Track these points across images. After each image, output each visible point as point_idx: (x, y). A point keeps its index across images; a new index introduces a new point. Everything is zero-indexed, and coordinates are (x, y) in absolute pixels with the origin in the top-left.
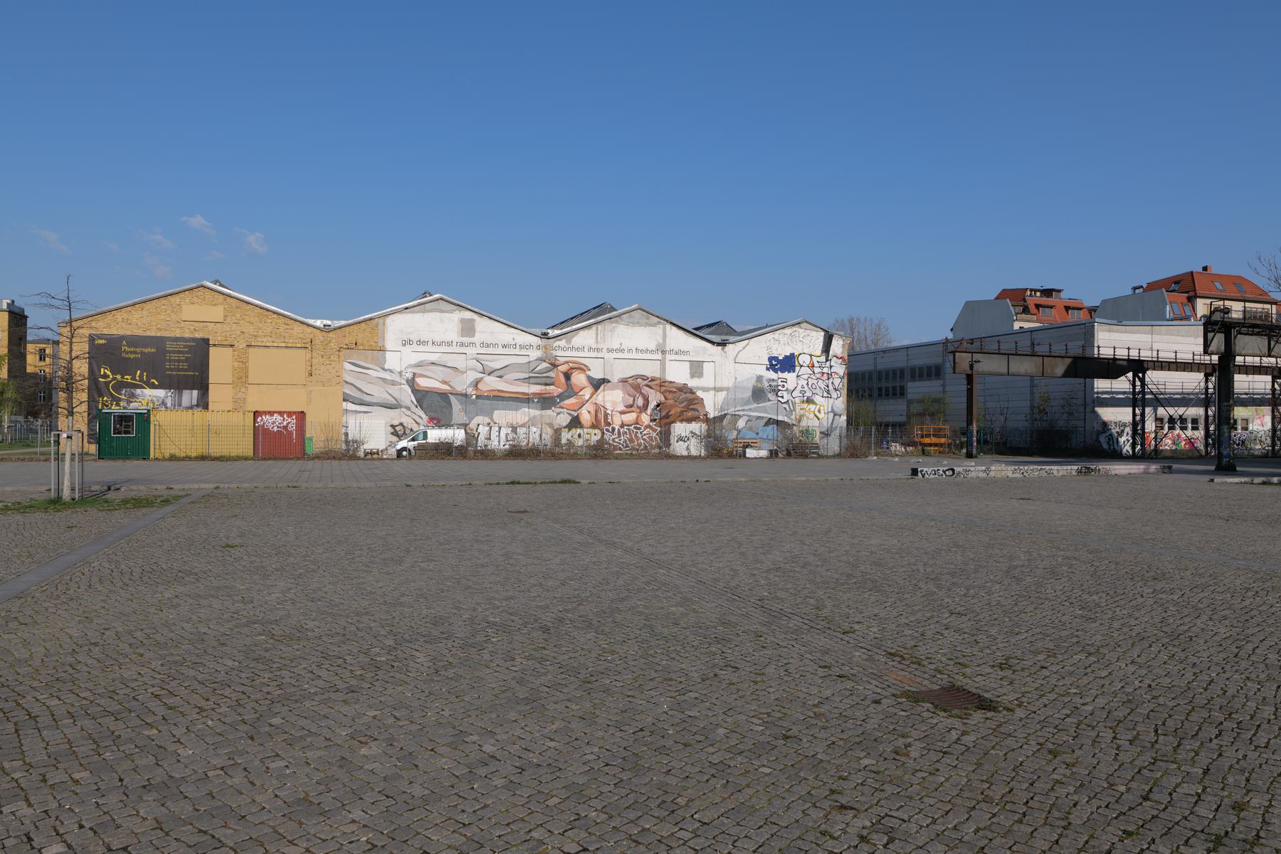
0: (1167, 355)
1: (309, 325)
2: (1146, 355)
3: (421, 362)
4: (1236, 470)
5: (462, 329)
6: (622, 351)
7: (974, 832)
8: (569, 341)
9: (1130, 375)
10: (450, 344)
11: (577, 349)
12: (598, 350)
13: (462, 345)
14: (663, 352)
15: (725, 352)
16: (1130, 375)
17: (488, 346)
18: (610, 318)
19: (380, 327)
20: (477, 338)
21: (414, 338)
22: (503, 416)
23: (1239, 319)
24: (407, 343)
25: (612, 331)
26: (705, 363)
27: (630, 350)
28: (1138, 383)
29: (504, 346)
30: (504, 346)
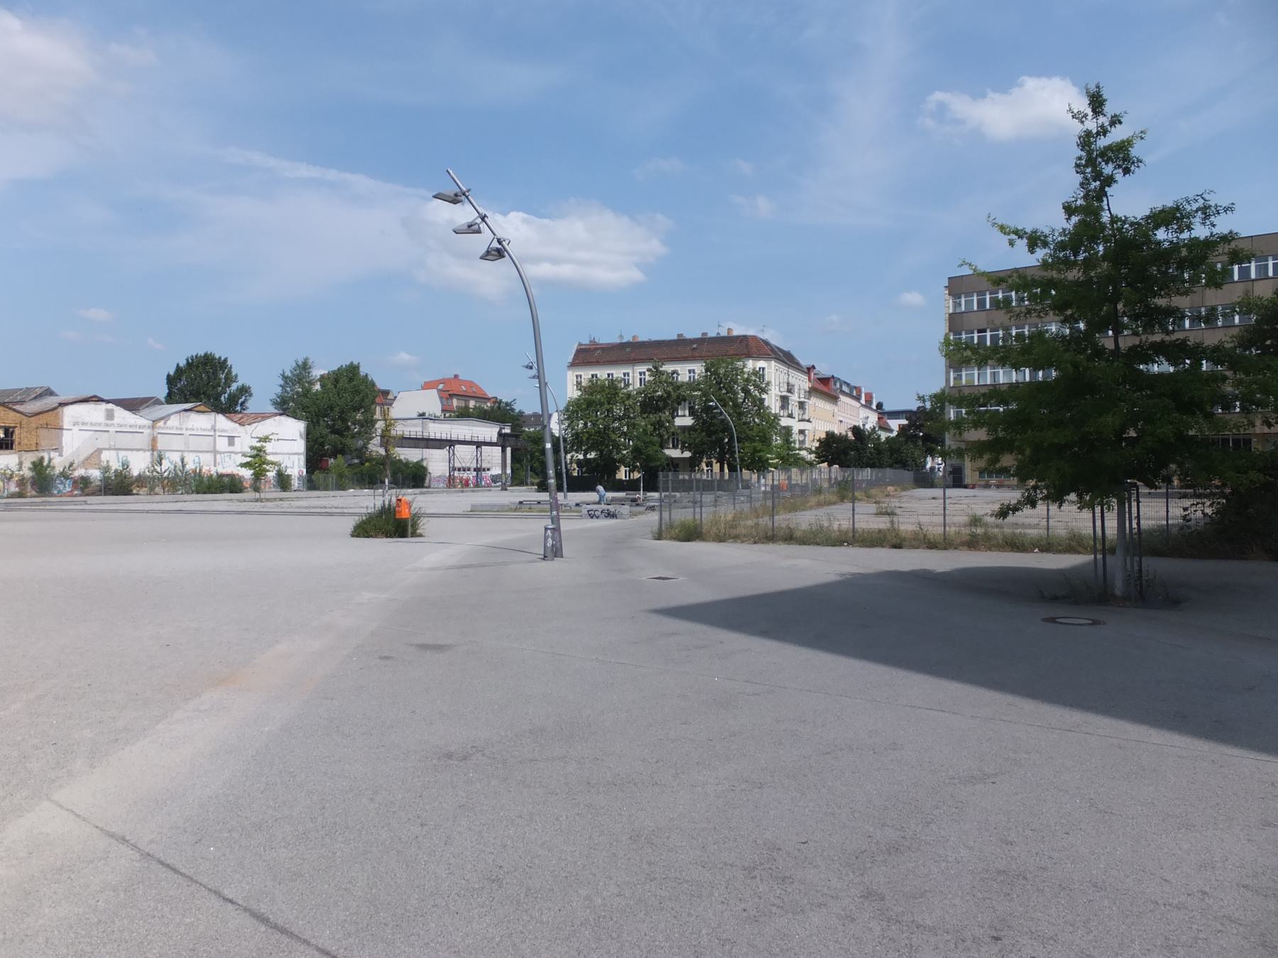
0: (461, 438)
1: (15, 410)
2: (454, 437)
3: (22, 404)
4: (537, 485)
5: (107, 415)
6: (193, 430)
7: (893, 939)
8: (165, 423)
9: (448, 448)
10: (100, 425)
11: (170, 428)
12: (181, 429)
13: (107, 425)
14: (215, 431)
15: (427, 386)
16: (448, 448)
17: (121, 426)
18: (102, 504)
19: (61, 412)
20: (116, 421)
21: (80, 420)
22: (1098, 545)
23: (814, 397)
24: (75, 424)
25: (188, 417)
26: (236, 439)
27: (197, 429)
28: (451, 451)
29: (130, 426)
30: (130, 426)
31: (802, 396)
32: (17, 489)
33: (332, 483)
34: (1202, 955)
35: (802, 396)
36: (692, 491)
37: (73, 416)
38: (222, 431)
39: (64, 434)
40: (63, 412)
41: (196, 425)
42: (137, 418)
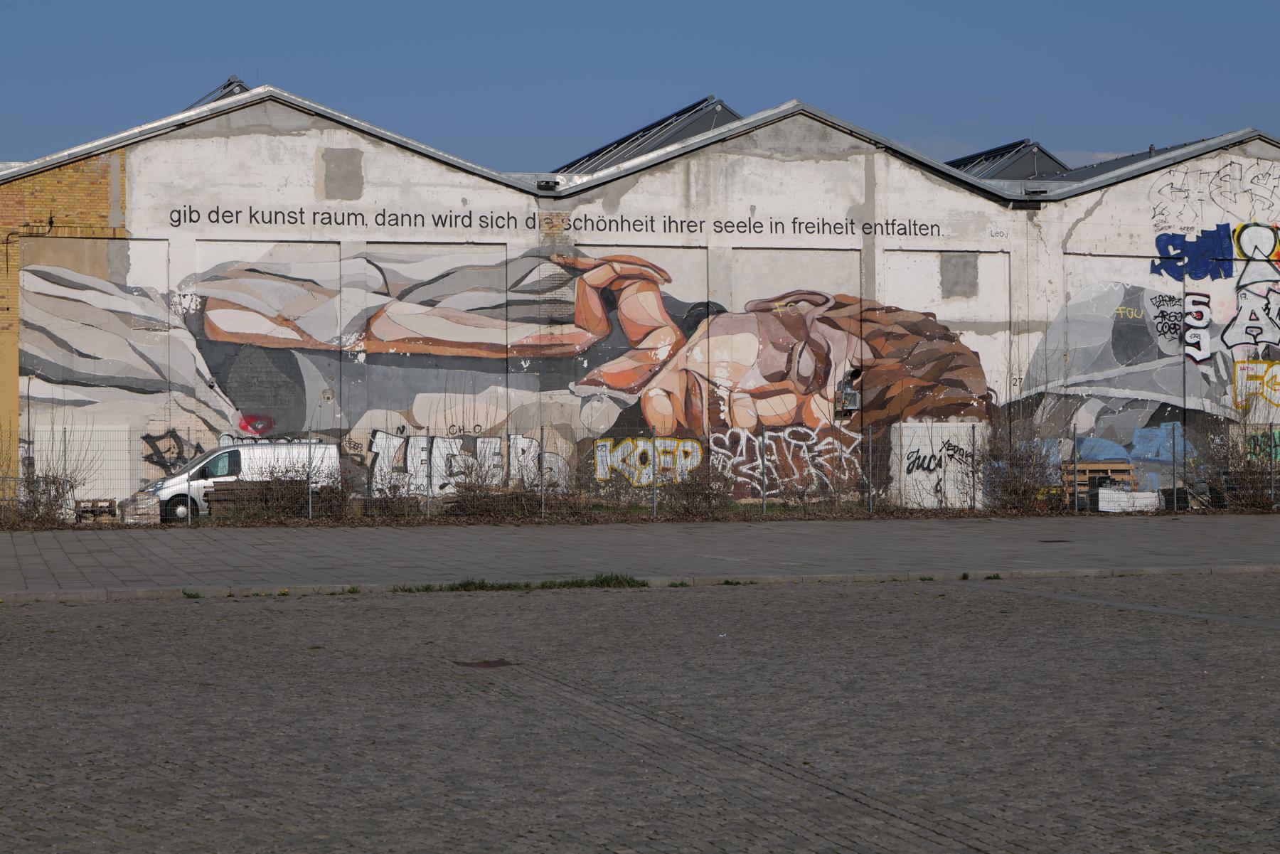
5: (329, 178)
6: (756, 227)
8: (612, 205)
11: (635, 225)
12: (691, 226)
13: (328, 219)
14: (868, 229)
19: (113, 177)
20: (369, 201)
21: (203, 203)
24: (182, 217)
25: (729, 173)
27: (776, 226)
29: (439, 221)
30: (439, 221)
31: (1081, 495)
32: (601, 473)
33: (467, 795)
34: (997, 465)
35: (1081, 495)
36: (1178, 489)
37: (168, 187)
38: (904, 231)
39: (1100, 496)
40: (123, 168)
41: (768, 208)
42: (475, 188)
